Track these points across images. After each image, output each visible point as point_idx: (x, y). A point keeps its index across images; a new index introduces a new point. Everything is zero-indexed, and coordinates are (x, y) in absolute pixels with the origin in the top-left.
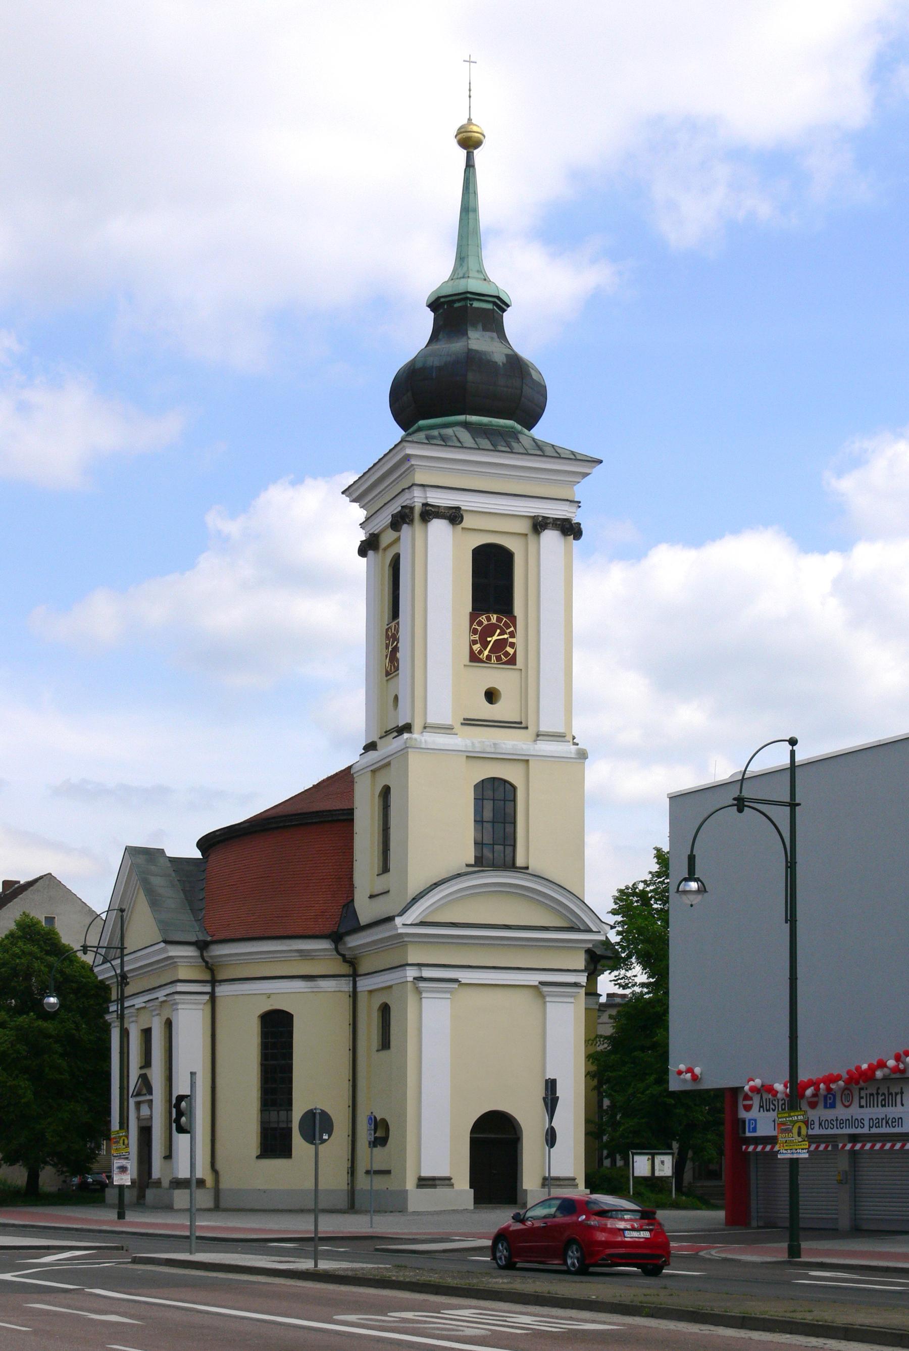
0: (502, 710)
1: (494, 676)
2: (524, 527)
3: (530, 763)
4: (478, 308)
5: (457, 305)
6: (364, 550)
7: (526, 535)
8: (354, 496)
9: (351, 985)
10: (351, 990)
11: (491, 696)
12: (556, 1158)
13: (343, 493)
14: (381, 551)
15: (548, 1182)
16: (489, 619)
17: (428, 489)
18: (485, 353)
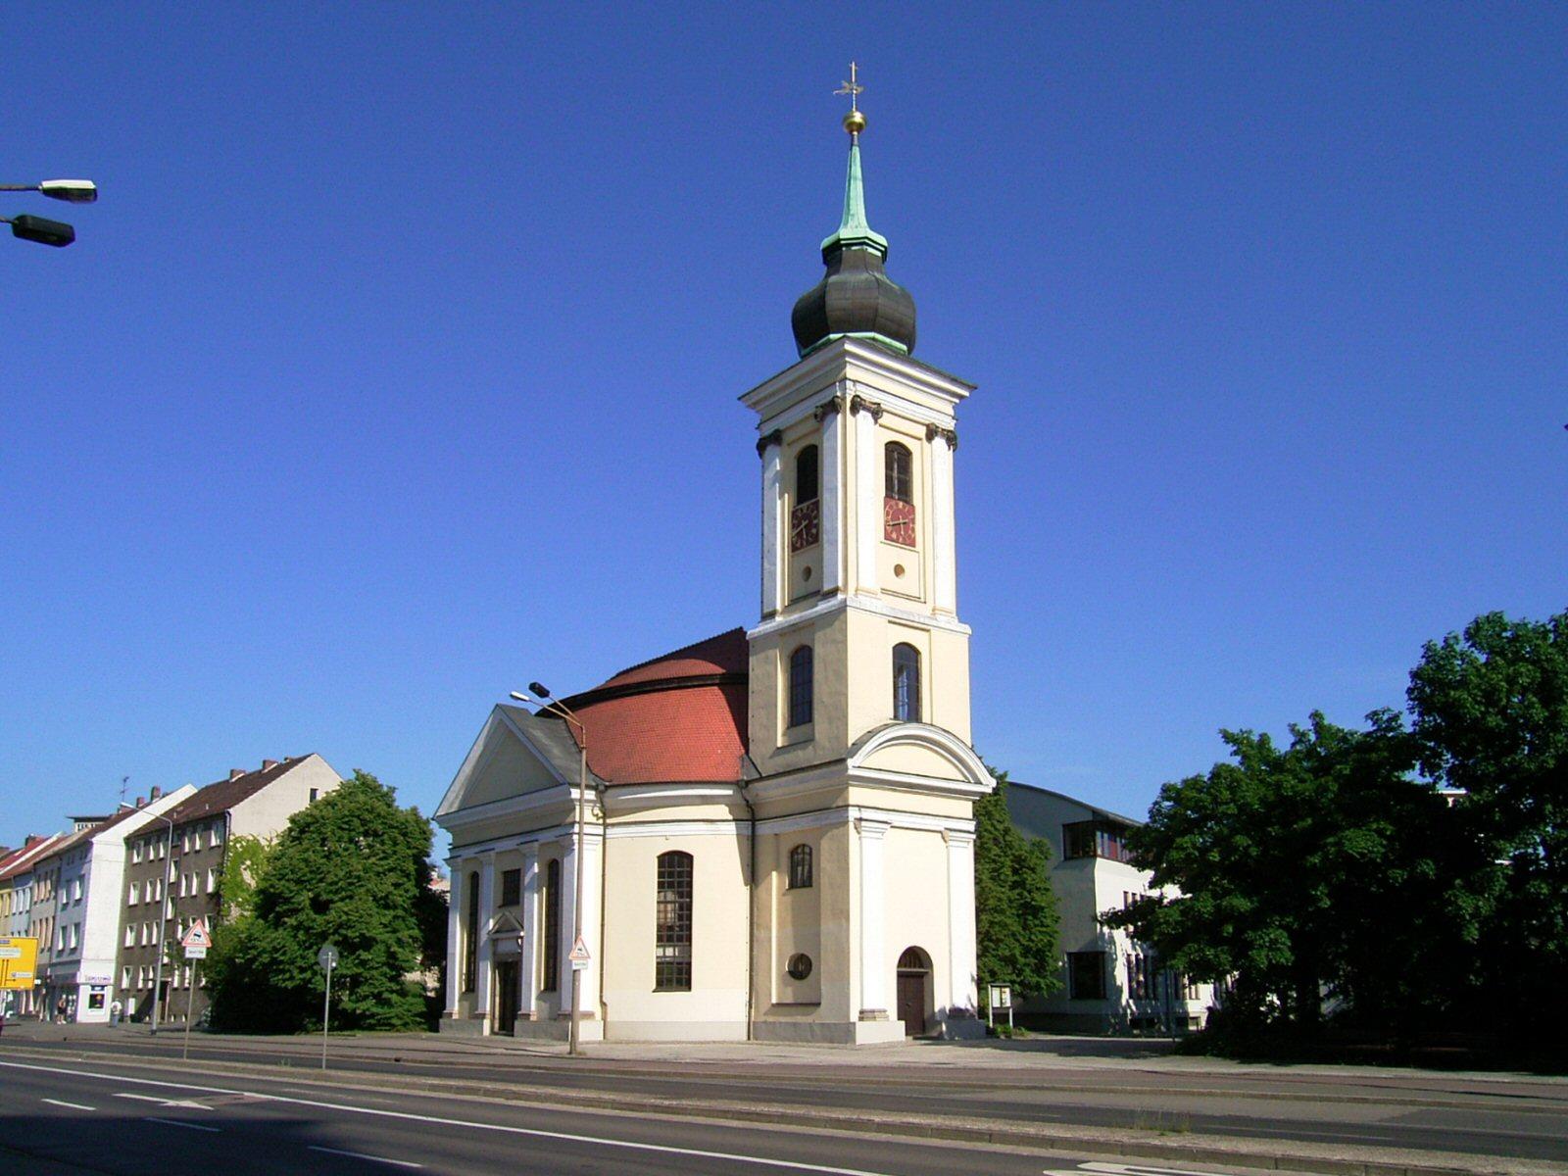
0: (908, 584)
1: (897, 554)
2: (922, 432)
3: (932, 632)
4: (870, 253)
5: (854, 248)
6: (761, 447)
7: (920, 439)
8: (750, 403)
9: (750, 828)
10: (750, 833)
11: (899, 570)
12: (955, 985)
13: (739, 399)
14: (785, 444)
15: (993, 1008)
16: (897, 504)
17: (858, 384)
18: (798, 303)
